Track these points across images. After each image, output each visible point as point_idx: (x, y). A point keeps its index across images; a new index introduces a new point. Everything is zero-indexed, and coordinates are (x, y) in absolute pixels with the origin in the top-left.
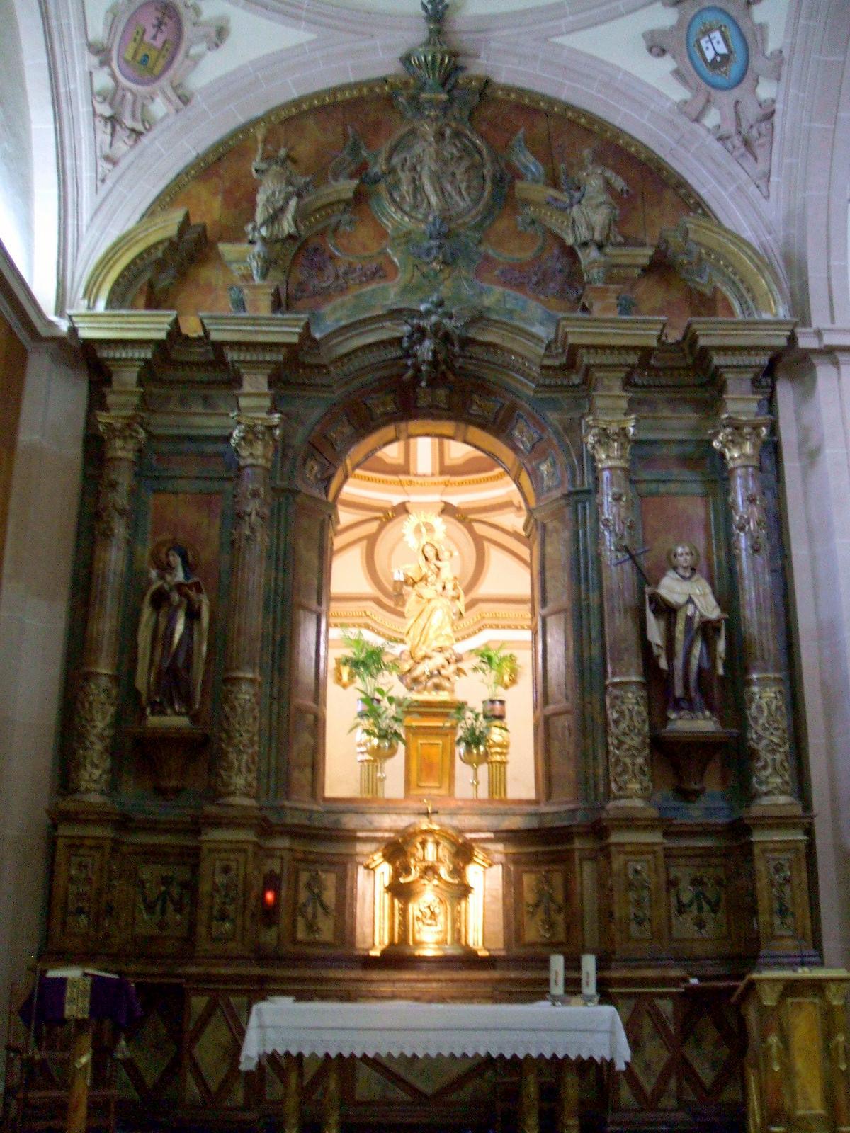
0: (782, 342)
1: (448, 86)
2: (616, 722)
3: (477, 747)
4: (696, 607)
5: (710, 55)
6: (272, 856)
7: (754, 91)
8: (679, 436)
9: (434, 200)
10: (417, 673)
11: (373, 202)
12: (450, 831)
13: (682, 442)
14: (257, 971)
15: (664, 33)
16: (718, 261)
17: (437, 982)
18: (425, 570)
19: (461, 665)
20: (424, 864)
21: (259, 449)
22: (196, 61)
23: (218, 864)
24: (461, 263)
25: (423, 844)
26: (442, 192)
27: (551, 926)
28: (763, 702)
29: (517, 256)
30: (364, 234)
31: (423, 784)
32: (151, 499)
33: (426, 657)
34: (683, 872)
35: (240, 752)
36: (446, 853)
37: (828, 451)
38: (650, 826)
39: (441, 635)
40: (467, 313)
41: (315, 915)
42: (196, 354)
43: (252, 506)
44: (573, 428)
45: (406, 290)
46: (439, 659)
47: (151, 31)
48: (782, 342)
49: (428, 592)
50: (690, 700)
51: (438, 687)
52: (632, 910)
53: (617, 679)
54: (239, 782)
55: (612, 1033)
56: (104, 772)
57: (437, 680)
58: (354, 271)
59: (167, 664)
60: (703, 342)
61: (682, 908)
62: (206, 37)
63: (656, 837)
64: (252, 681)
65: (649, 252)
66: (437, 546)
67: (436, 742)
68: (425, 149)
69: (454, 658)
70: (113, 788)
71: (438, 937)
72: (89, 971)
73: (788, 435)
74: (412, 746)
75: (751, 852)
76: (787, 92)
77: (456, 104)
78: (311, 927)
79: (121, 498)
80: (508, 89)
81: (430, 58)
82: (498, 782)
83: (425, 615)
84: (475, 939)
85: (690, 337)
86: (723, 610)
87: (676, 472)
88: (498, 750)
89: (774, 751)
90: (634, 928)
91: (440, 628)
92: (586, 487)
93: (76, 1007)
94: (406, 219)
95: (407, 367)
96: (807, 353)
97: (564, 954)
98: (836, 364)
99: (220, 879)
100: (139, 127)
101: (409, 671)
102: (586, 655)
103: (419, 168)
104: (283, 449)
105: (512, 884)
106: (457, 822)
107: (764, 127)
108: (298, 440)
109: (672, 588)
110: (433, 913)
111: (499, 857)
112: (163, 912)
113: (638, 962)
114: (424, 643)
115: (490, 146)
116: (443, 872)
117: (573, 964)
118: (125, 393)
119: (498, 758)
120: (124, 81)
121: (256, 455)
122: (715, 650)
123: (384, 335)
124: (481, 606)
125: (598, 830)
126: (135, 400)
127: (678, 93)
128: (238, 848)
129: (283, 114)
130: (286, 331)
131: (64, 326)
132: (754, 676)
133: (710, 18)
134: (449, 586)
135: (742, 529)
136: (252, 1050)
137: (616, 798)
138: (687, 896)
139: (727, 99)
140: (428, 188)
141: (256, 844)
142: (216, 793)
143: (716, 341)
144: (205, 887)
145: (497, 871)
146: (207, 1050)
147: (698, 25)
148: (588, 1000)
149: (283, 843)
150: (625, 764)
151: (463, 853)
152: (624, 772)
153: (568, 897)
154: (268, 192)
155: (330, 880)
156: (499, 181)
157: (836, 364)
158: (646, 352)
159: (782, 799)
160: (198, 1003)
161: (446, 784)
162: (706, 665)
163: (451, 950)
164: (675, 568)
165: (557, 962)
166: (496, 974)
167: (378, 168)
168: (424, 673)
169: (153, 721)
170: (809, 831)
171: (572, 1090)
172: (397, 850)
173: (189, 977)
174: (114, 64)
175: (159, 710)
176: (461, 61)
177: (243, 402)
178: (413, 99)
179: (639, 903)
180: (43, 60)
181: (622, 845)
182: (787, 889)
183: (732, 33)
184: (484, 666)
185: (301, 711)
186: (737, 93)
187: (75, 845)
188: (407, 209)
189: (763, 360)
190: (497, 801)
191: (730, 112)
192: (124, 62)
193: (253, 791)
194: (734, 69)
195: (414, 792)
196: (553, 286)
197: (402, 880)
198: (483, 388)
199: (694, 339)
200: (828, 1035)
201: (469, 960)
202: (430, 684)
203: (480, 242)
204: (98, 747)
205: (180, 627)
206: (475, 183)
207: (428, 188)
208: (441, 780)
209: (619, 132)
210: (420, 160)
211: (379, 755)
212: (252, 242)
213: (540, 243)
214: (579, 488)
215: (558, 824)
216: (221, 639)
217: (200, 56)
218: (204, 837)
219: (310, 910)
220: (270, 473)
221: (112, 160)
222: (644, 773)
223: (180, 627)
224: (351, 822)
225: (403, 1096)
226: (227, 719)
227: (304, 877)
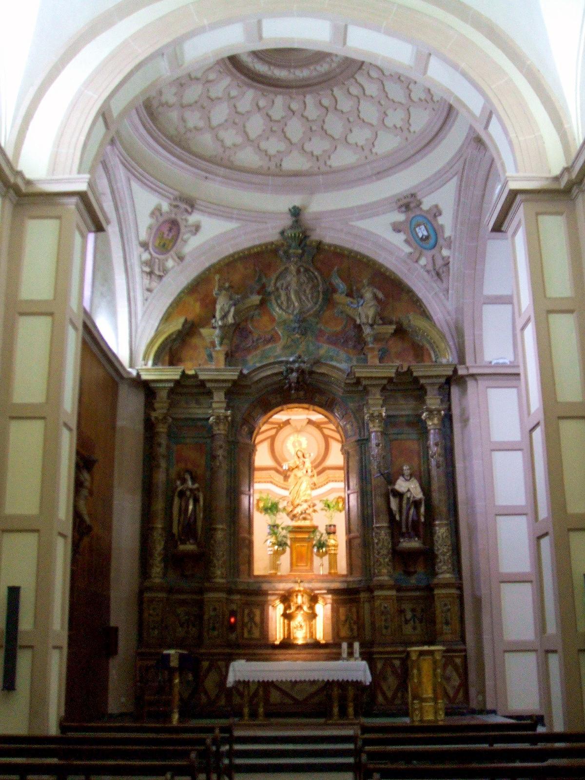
0: (450, 373)
1: (302, 246)
2: (377, 544)
3: (322, 549)
4: (411, 493)
5: (420, 235)
6: (233, 603)
7: (440, 252)
8: (407, 413)
9: (296, 304)
10: (295, 512)
11: (269, 304)
12: (308, 591)
13: (408, 416)
14: (228, 650)
15: (401, 223)
16: (424, 333)
17: (304, 653)
18: (298, 463)
19: (315, 508)
20: (297, 605)
21: (222, 427)
22: (185, 242)
23: (211, 608)
24: (309, 333)
25: (297, 596)
26: (300, 300)
27: (352, 630)
28: (440, 534)
29: (335, 330)
30: (265, 319)
31: (299, 565)
32: (175, 448)
33: (298, 505)
34: (407, 606)
35: (218, 560)
36: (307, 600)
37: (471, 421)
38: (390, 588)
39: (305, 494)
40: (312, 361)
41: (251, 627)
42: (191, 382)
43: (220, 453)
44: (360, 410)
45: (285, 347)
46: (305, 506)
47: (167, 233)
48: (450, 373)
49: (299, 473)
50: (408, 533)
51: (305, 519)
52: (383, 623)
53: (378, 525)
54: (219, 572)
55: (365, 671)
56: (161, 570)
57: (304, 516)
58: (261, 338)
59: (187, 522)
60: (415, 374)
61: (407, 622)
62: (191, 231)
63: (393, 593)
64: (222, 529)
65: (394, 327)
66: (303, 451)
67: (304, 545)
68: (292, 279)
69: (312, 505)
70: (165, 575)
71: (304, 635)
72: (178, 651)
73: (456, 412)
74: (294, 547)
75: (433, 598)
76: (454, 254)
77: (306, 254)
78: (250, 632)
79: (162, 450)
80: (330, 246)
81: (293, 235)
82: (333, 563)
83: (298, 484)
84: (320, 636)
85: (409, 372)
86: (424, 494)
87: (407, 429)
88: (333, 548)
89: (444, 555)
90: (384, 631)
91: (305, 491)
92: (366, 437)
93: (174, 663)
94: (284, 313)
95: (285, 384)
96: (462, 377)
97: (359, 642)
98: (476, 380)
99: (212, 613)
100: (162, 274)
101: (291, 511)
102: (366, 513)
103: (289, 288)
104: (233, 424)
105: (335, 611)
106: (311, 585)
107: (445, 269)
108: (238, 419)
109: (401, 485)
110: (301, 626)
111: (329, 601)
112: (188, 627)
113: (384, 645)
114: (298, 498)
115: (321, 274)
116: (305, 608)
117: (350, 646)
118: (162, 402)
119: (333, 552)
120: (154, 255)
121: (221, 430)
122: (420, 512)
123: (276, 371)
124: (328, 472)
125: (370, 590)
126: (166, 405)
127: (408, 249)
128: (219, 600)
129: (227, 261)
130: (232, 375)
131: (134, 373)
132: (437, 522)
133: (420, 220)
134: (309, 471)
135: (432, 457)
136: (231, 680)
137: (377, 576)
138: (409, 615)
139: (429, 253)
140: (293, 297)
141: (227, 599)
142: (209, 578)
143: (420, 374)
144: (206, 617)
145: (329, 606)
146: (210, 683)
147: (414, 223)
148: (356, 659)
149: (236, 597)
150: (381, 563)
151: (314, 599)
152: (380, 565)
153: (358, 618)
154: (222, 304)
155: (257, 612)
156: (325, 293)
157: (476, 380)
158: (390, 380)
159: (448, 576)
160: (205, 664)
161: (309, 564)
162: (415, 518)
163: (309, 641)
164: (403, 475)
165: (345, 645)
166: (327, 651)
167: (271, 289)
168: (298, 513)
169: (182, 547)
170: (460, 588)
171: (351, 692)
172: (286, 599)
173: (202, 654)
174: (151, 248)
175: (184, 542)
176: (308, 233)
177: (214, 405)
178: (286, 252)
179: (386, 620)
180: (121, 254)
181: (380, 596)
182: (449, 614)
183: (429, 227)
184: (326, 508)
185: (244, 539)
186: (434, 251)
187: (151, 600)
188: (284, 308)
189: (443, 380)
190: (332, 576)
191: (430, 259)
192: (155, 247)
193: (224, 576)
194: (432, 241)
195: (295, 568)
196: (351, 344)
197: (288, 612)
198: (321, 392)
199: (412, 373)
200: (435, 670)
201: (316, 645)
202: (301, 517)
203: (317, 323)
204: (159, 559)
205: (191, 507)
206: (315, 294)
207: (293, 297)
208: (307, 563)
209: (381, 266)
210: (289, 285)
211: (277, 554)
212: (214, 328)
213: (344, 322)
214: (362, 438)
215: (354, 586)
216: (209, 509)
217: (188, 239)
218: (205, 596)
219: (249, 625)
220: (226, 436)
221: (149, 290)
222: (388, 565)
223: (191, 507)
224: (265, 586)
225: (291, 702)
226: (213, 546)
227: (246, 611)
